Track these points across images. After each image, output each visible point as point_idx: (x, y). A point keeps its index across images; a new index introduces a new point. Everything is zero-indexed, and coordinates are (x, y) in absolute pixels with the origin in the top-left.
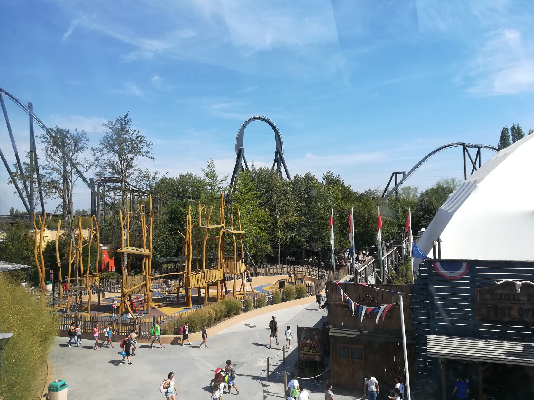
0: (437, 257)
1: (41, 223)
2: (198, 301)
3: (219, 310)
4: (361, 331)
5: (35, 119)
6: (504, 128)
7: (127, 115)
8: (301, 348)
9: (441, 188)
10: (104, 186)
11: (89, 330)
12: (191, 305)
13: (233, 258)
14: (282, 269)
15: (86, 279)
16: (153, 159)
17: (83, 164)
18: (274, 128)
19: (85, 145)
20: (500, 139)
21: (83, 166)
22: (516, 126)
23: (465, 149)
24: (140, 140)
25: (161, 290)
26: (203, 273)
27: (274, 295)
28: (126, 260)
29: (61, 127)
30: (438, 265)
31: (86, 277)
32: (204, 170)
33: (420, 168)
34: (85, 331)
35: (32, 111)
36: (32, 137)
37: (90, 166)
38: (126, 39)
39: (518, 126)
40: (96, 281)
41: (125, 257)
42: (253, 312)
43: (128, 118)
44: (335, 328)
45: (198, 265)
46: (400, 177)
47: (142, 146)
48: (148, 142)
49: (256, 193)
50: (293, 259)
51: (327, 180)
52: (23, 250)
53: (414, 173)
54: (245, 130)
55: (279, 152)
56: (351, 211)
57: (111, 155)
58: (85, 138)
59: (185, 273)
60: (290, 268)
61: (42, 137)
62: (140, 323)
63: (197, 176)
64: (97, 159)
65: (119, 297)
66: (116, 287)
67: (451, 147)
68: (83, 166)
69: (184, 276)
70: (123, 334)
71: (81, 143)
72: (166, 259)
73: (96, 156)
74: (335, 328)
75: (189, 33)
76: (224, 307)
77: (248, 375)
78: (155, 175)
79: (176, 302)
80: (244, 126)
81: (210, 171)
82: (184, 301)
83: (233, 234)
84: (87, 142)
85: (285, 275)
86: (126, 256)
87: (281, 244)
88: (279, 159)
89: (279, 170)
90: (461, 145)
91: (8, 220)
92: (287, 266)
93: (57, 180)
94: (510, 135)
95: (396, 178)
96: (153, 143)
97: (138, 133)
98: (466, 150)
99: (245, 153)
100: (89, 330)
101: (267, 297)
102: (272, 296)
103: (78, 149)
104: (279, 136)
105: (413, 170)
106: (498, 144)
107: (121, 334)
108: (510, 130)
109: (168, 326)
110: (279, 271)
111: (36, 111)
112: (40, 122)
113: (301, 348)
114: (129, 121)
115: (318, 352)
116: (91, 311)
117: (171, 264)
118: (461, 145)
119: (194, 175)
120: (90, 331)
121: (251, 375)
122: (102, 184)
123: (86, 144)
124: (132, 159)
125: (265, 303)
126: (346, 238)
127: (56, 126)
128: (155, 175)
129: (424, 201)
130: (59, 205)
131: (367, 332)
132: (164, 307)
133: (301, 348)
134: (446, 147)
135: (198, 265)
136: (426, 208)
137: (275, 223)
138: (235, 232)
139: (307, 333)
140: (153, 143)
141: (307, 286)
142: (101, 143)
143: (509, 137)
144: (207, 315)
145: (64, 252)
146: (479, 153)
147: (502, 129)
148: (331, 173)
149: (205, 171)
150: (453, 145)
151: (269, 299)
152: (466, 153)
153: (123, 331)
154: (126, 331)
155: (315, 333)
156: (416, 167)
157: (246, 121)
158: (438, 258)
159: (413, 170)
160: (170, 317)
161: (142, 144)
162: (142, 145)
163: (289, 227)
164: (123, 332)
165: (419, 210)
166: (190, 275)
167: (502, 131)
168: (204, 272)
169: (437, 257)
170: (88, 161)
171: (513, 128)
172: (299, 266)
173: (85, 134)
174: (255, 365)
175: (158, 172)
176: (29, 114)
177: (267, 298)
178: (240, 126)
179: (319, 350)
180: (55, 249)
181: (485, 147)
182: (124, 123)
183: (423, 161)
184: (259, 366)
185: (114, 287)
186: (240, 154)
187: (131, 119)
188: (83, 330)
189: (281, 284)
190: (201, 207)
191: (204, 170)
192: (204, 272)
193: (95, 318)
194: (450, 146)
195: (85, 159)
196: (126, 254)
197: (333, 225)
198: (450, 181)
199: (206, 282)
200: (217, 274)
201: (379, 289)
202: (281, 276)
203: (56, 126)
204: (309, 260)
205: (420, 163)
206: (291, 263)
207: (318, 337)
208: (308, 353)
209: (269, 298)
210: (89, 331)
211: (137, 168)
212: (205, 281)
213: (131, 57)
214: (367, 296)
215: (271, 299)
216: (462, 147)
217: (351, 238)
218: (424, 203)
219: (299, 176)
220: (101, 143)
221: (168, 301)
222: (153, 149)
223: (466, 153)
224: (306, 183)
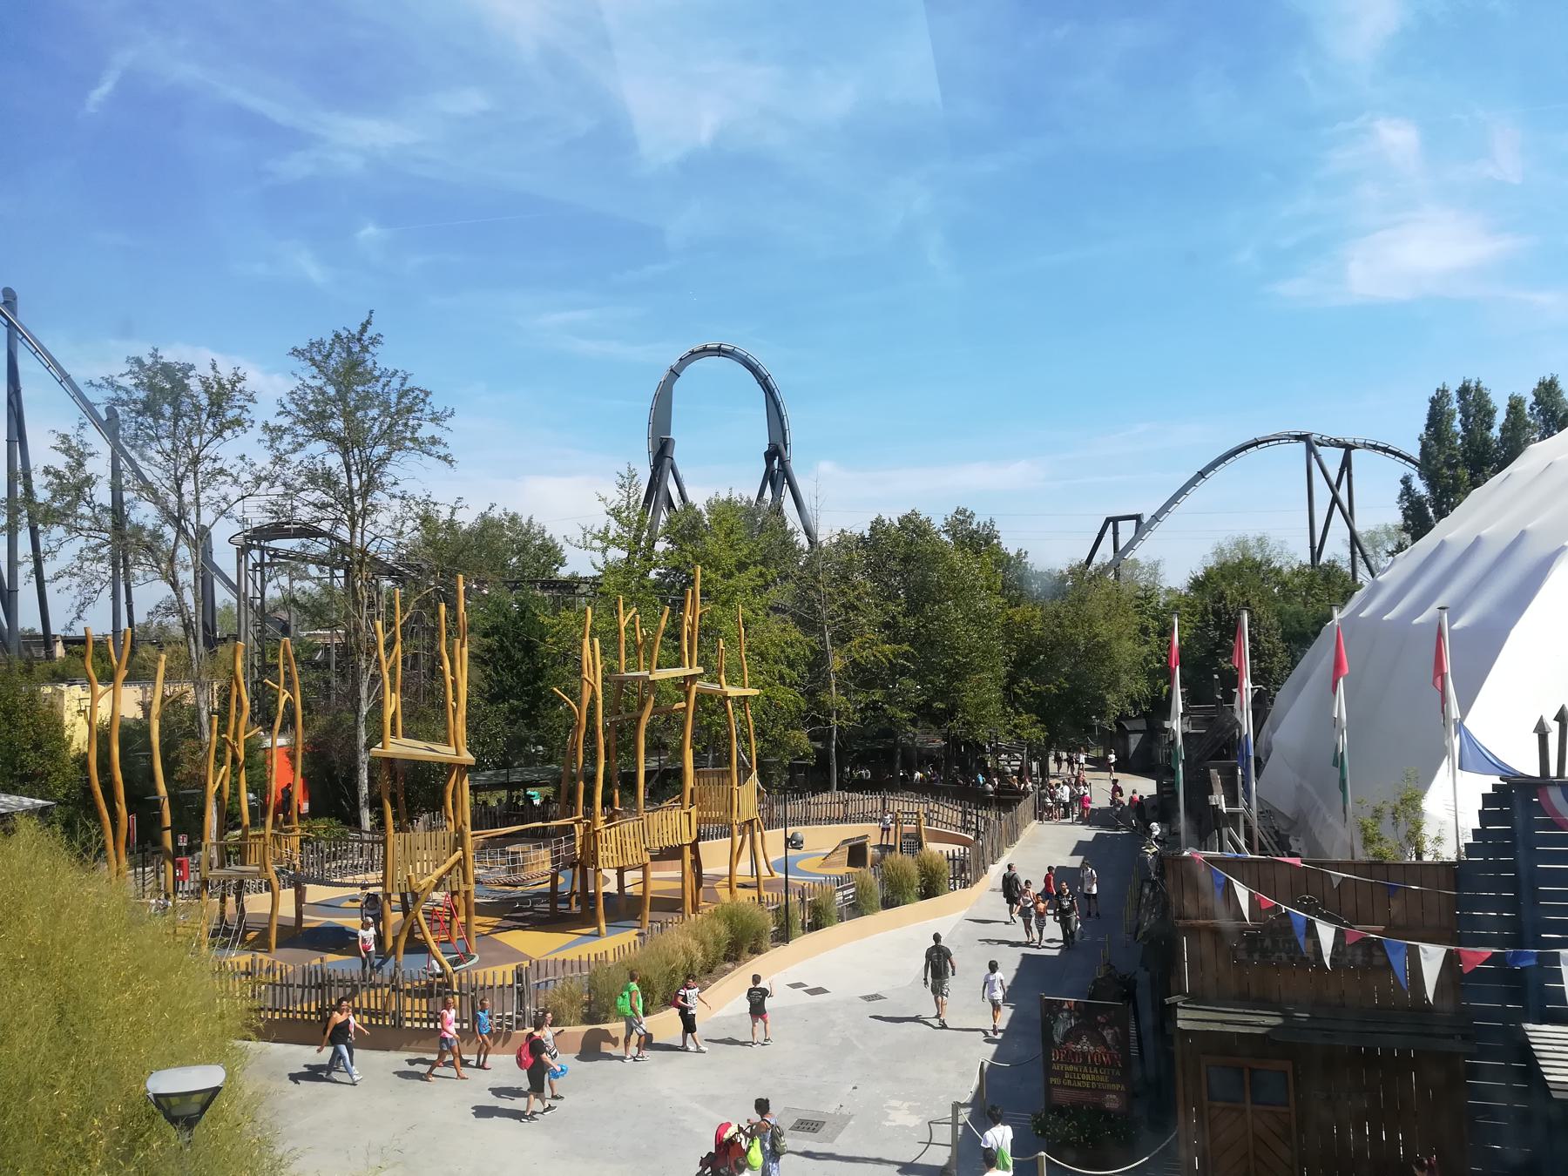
0: (1553, 772)
1: (115, 662)
2: (624, 909)
3: (709, 938)
4: (1286, 1016)
5: (24, 340)
6: (1438, 390)
7: (368, 322)
8: (1056, 1067)
9: (1249, 564)
10: (262, 549)
11: (298, 1012)
12: (603, 924)
13: (729, 773)
14: (846, 805)
15: (265, 845)
16: (450, 462)
17: (235, 475)
19: (245, 415)
20: (1426, 422)
21: (236, 481)
22: (1473, 385)
23: (1310, 449)
24: (410, 403)
25: (487, 876)
27: (857, 889)
28: (366, 781)
29: (169, 356)
30: (1555, 795)
31: (263, 836)
32: (604, 500)
33: (1186, 502)
34: (285, 1015)
35: (14, 313)
36: (14, 396)
37: (258, 480)
38: (279, 114)
39: (1478, 383)
40: (292, 850)
41: (361, 771)
42: (803, 943)
43: (371, 332)
44: (1194, 1006)
45: (617, 795)
46: (1127, 530)
47: (416, 422)
48: (439, 408)
49: (764, 570)
50: (866, 773)
51: (954, 535)
52: (24, 750)
53: (1167, 519)
54: (678, 386)
55: (775, 453)
56: (1238, 621)
57: (318, 447)
58: (240, 391)
59: (578, 821)
60: (871, 802)
62: (474, 990)
63: (534, 521)
64: (280, 459)
65: (351, 900)
66: (340, 867)
67: (1271, 443)
68: (236, 481)
69: (574, 832)
70: (417, 1025)
71: (232, 407)
72: (484, 776)
73: (278, 450)
74: (1194, 1006)
75: (472, 101)
76: (723, 930)
77: (879, 1161)
78: (453, 513)
79: (546, 913)
80: (675, 373)
81: (624, 503)
82: (570, 908)
83: (726, 698)
84: (250, 406)
85: (857, 825)
86: (366, 766)
87: (840, 728)
88: (777, 470)
89: (778, 510)
90: (1299, 438)
91: (34, 651)
92: (861, 796)
93: (155, 525)
94: (1455, 410)
95: (1116, 534)
97: (405, 379)
99: (679, 454)
100: (298, 1012)
101: (840, 893)
102: (853, 890)
103: (223, 427)
104: (777, 406)
105: (1165, 509)
106: (1421, 436)
107: (408, 1024)
108: (1454, 396)
109: (563, 996)
110: (838, 810)
111: (23, 317)
112: (40, 351)
113: (1054, 1067)
114: (374, 341)
115: (1113, 1080)
116: (278, 946)
117: (503, 794)
118: (1299, 438)
119: (524, 521)
120: (303, 1017)
121: (845, 1154)
122: (255, 542)
123: (247, 410)
124: (383, 461)
125: (835, 914)
126: (1021, 710)
127: (151, 351)
128: (453, 513)
130: (158, 606)
131: (1307, 1015)
132: (509, 929)
133: (1054, 1067)
134: (1256, 443)
135: (617, 795)
136: (1230, 619)
137: (818, 662)
138: (733, 692)
139: (1077, 1019)
141: (948, 859)
142: (282, 409)
143: (1452, 415)
144: (681, 959)
145: (178, 756)
146: (1346, 464)
147: (1433, 393)
148: (968, 514)
149: (608, 501)
151: (845, 901)
152: (1314, 462)
153: (417, 1015)
154: (421, 1015)
155: (1103, 1020)
156: (1174, 499)
157: (681, 359)
158: (1555, 775)
159: (1165, 509)
160: (568, 966)
161: (419, 415)
162: (419, 419)
163: (862, 676)
164: (416, 1020)
165: (1209, 625)
167: (1433, 398)
169: (1553, 772)
170: (252, 466)
171: (1464, 391)
172: (867, 794)
173: (244, 379)
174: (887, 1124)
175: (463, 503)
176: (6, 322)
177: (839, 897)
178: (663, 375)
179: (1118, 1073)
180: (148, 746)
181: (1365, 446)
182: (356, 348)
183: (1192, 483)
184: (900, 1126)
185: (334, 865)
186: (662, 453)
187: (380, 335)
188: (277, 1013)
189: (856, 854)
190: (626, 615)
191: (604, 500)
193: (320, 976)
194: (1268, 441)
195: (242, 458)
196: (364, 763)
197: (1178, 667)
198: (1252, 543)
199: (646, 849)
200: (673, 823)
201: (1345, 875)
202: (861, 825)
203: (151, 351)
204: (913, 775)
205: (1183, 491)
206: (858, 786)
207: (1115, 1032)
208: (1079, 1084)
209: (844, 897)
210: (299, 1016)
211: (396, 490)
212: (644, 847)
213: (296, 166)
214: (1305, 899)
215: (849, 900)
216: (1302, 445)
217: (1242, 709)
218: (1225, 605)
219: (887, 522)
220: (282, 409)
221: (519, 910)
222: (454, 435)
223: (1314, 462)
224: (906, 543)
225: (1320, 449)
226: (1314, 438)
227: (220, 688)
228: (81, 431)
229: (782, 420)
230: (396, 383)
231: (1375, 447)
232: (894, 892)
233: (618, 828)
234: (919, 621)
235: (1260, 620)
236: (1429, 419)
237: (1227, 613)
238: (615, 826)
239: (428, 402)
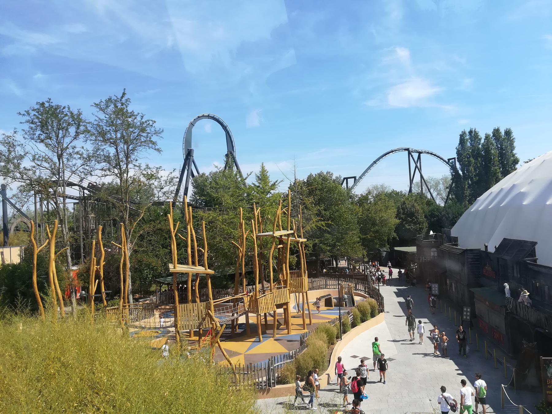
6: (462, 132)
18: (225, 128)
20: (459, 143)
22: (473, 130)
23: (409, 153)
26: (272, 293)
32: (217, 167)
46: (351, 182)
53: (364, 178)
54: (194, 130)
61: (26, 114)
75: (79, 28)
80: (192, 124)
90: (405, 150)
92: (318, 279)
95: (347, 183)
96: (163, 131)
97: (142, 117)
98: (411, 155)
99: (196, 156)
102: (352, 316)
105: (363, 174)
106: (457, 147)
108: (468, 134)
118: (405, 150)
129: (405, 204)
134: (392, 152)
136: (408, 210)
140: (163, 131)
146: (419, 158)
147: (461, 133)
150: (399, 150)
152: (411, 158)
157: (194, 120)
159: (363, 174)
166: (258, 297)
168: (273, 293)
171: (470, 132)
181: (425, 152)
183: (372, 165)
186: (189, 155)
192: (273, 293)
194: (396, 151)
212: (274, 304)
216: (407, 152)
223: (411, 158)
225: (412, 153)
226: (410, 149)
227: (24, 248)
228: (15, 135)
229: (232, 143)
230: (139, 118)
231: (428, 153)
232: (363, 316)
233: (263, 297)
234: (330, 213)
235: (418, 211)
236: (460, 142)
237: (407, 209)
238: (265, 296)
239: (153, 126)
